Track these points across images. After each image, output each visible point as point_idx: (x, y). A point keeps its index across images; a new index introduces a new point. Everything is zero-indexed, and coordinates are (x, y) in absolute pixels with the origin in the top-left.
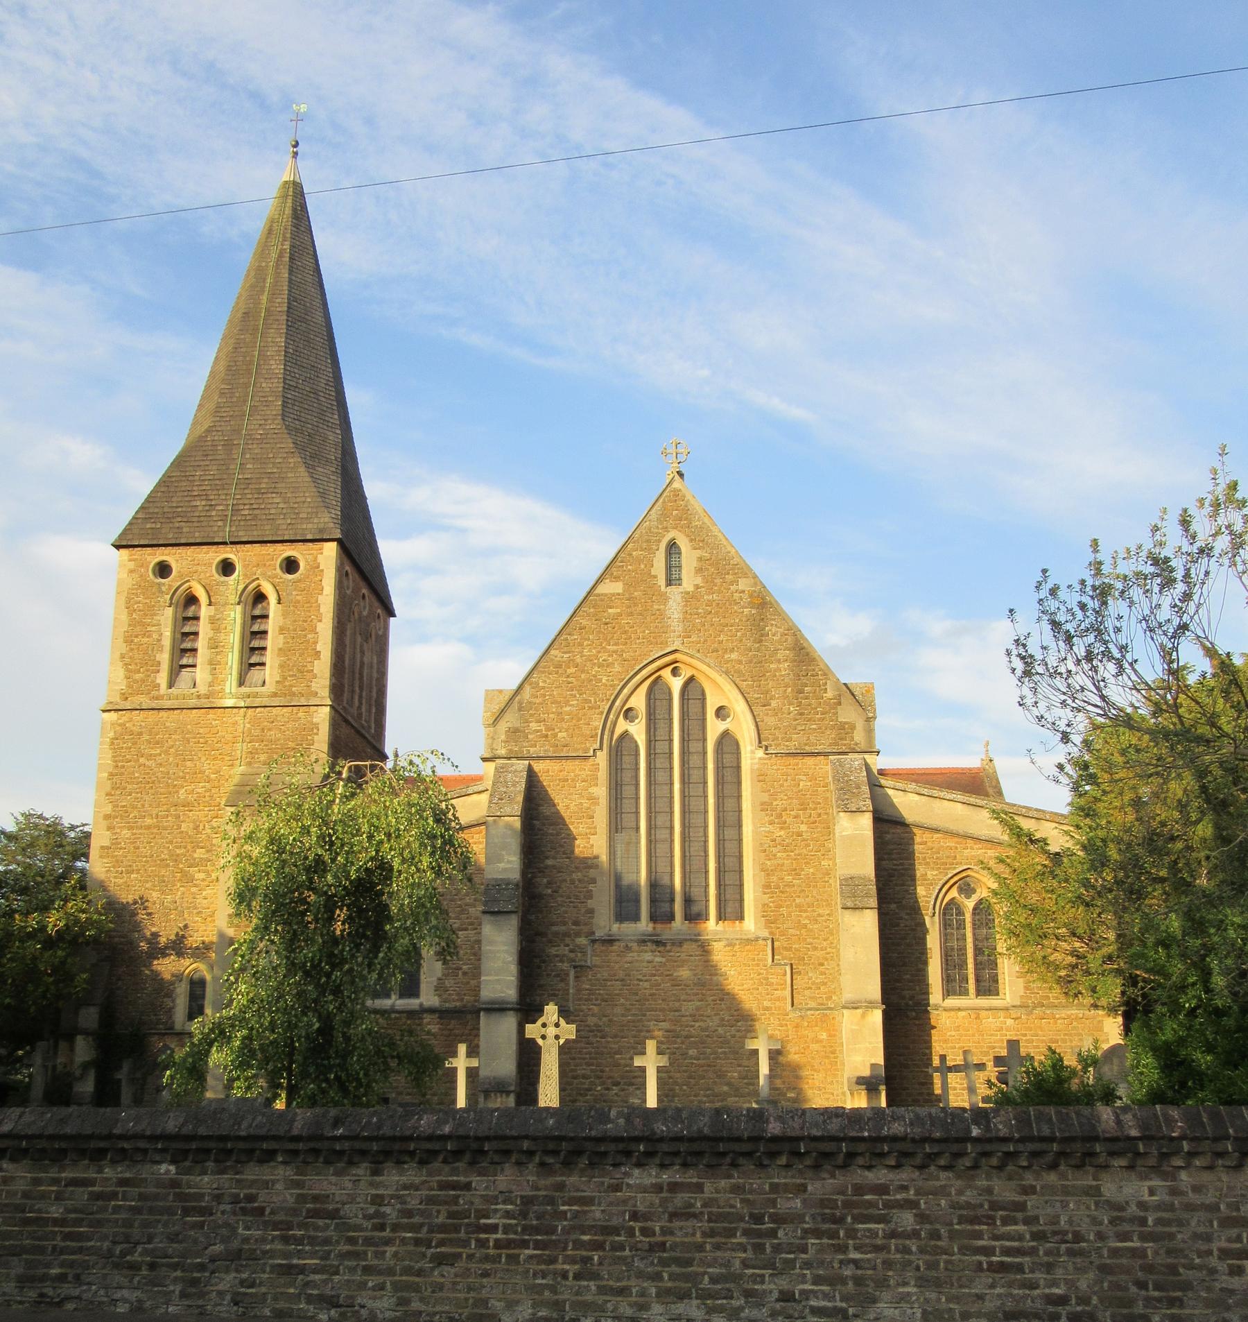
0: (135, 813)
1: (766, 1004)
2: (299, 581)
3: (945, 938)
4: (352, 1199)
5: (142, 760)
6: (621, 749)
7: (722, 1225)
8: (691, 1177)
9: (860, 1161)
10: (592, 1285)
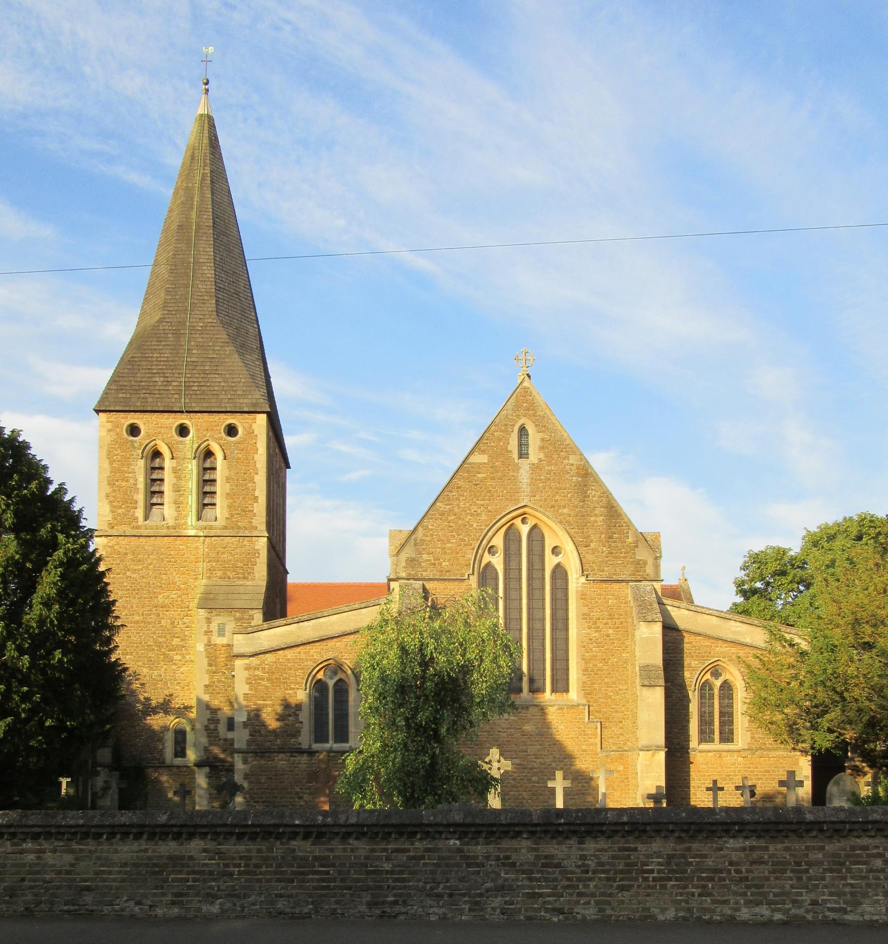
0: (126, 612)
1: (584, 747)
3: (701, 705)
4: (568, 857)
5: (128, 574)
6: (486, 575)
7: (779, 867)
8: (762, 843)
9: (855, 834)
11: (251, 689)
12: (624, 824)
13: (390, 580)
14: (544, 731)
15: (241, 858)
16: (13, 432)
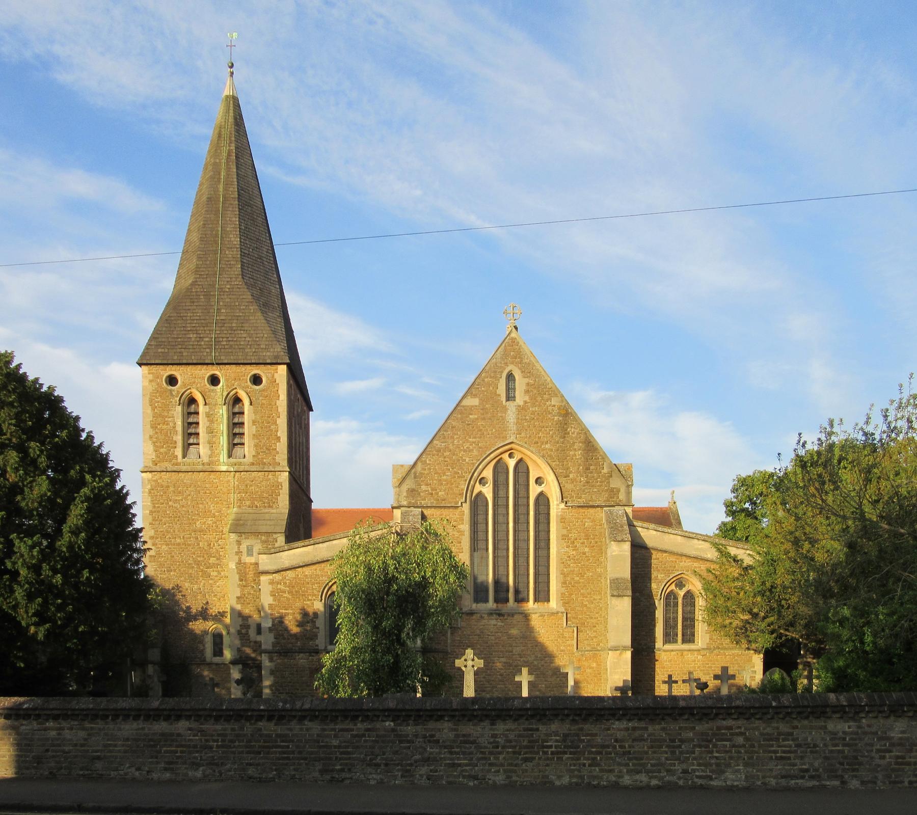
0: (170, 535)
2: (264, 390)
4: (482, 735)
5: (170, 503)
6: (478, 503)
8: (642, 724)
9: (721, 717)
10: (597, 769)
11: (274, 600)
12: (527, 709)
13: (393, 508)
14: (528, 634)
15: (219, 735)
16: (49, 388)
